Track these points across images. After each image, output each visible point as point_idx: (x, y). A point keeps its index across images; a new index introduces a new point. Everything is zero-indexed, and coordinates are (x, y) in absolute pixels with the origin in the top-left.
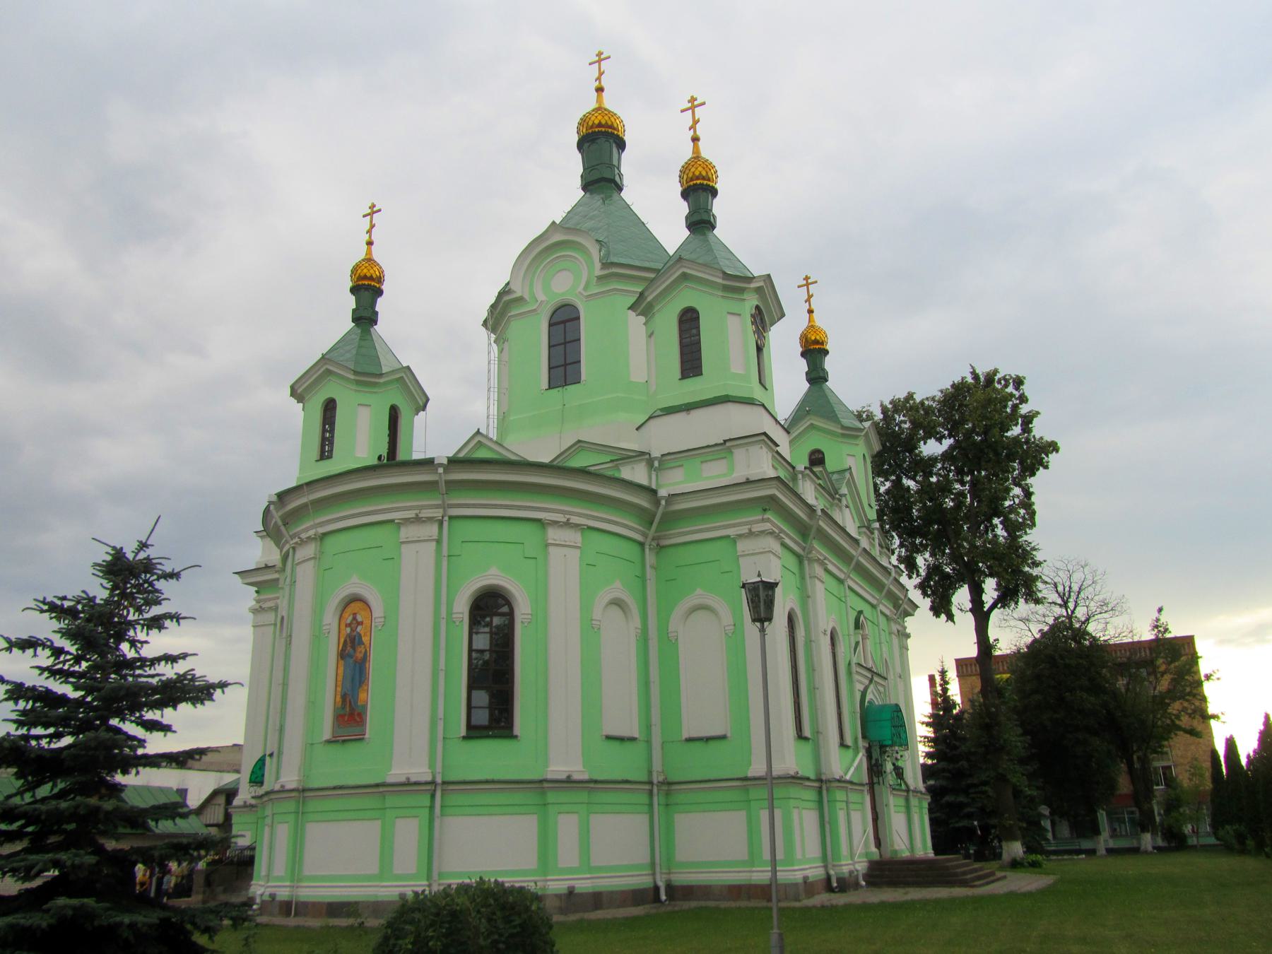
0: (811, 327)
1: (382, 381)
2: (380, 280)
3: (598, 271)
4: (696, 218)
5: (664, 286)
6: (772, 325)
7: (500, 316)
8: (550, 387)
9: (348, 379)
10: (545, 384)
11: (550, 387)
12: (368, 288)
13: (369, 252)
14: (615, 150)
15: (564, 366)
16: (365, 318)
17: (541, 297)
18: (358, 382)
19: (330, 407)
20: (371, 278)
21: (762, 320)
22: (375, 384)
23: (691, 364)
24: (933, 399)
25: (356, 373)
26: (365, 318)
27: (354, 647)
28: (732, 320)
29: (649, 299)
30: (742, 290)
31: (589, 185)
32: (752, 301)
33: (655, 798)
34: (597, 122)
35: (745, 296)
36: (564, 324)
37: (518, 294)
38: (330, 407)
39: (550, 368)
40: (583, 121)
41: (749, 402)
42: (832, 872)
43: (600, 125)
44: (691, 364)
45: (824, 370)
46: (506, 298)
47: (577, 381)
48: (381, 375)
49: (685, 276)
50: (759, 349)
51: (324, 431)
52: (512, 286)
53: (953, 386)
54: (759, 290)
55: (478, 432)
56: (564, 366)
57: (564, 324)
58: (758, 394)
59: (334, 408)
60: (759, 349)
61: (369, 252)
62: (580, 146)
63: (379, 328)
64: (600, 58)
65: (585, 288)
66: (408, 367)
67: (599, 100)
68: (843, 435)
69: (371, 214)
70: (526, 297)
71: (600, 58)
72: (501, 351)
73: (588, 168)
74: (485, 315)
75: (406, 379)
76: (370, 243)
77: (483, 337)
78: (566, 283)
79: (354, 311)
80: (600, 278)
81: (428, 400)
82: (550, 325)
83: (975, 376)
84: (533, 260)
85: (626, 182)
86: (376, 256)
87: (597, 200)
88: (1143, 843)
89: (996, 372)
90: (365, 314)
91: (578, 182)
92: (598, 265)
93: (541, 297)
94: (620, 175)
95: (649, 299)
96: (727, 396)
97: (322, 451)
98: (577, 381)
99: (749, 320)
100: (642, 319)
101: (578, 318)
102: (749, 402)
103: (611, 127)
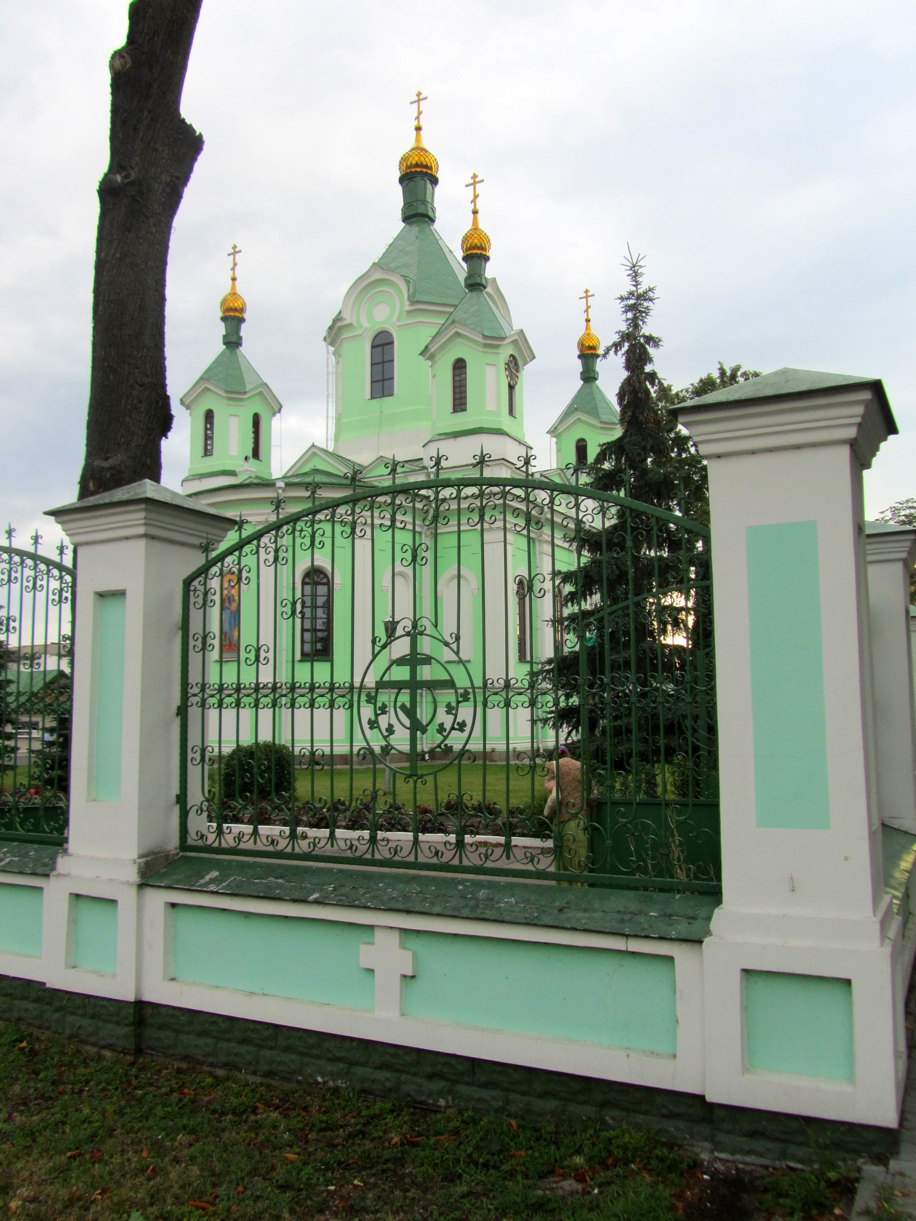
0: (588, 335)
1: (246, 397)
2: (242, 310)
3: (407, 307)
4: (471, 281)
5: (440, 343)
6: (525, 364)
7: (336, 333)
8: (372, 398)
9: (221, 396)
10: (369, 396)
11: (372, 398)
12: (234, 318)
13: (234, 287)
14: (429, 186)
15: (382, 382)
16: (233, 342)
17: (366, 324)
18: (229, 399)
19: (209, 416)
20: (236, 310)
21: (516, 364)
22: (241, 400)
23: (459, 403)
24: (687, 391)
25: (227, 392)
26: (233, 342)
27: (229, 603)
28: (490, 371)
29: (432, 351)
30: (497, 346)
31: (408, 218)
32: (506, 352)
33: (424, 698)
34: (414, 162)
35: (500, 351)
36: (382, 346)
37: (348, 322)
38: (209, 416)
39: (372, 382)
40: (404, 159)
41: (499, 432)
42: (541, 746)
43: (417, 165)
44: (459, 403)
45: (594, 371)
46: (339, 324)
47: (391, 394)
48: (245, 393)
49: (457, 334)
50: (511, 388)
51: (206, 429)
52: (343, 315)
53: (701, 381)
54: (515, 342)
55: (313, 446)
56: (382, 382)
57: (382, 346)
58: (505, 422)
59: (212, 417)
60: (511, 388)
61: (234, 287)
62: (401, 181)
63: (244, 349)
64: (419, 99)
65: (398, 320)
66: (266, 384)
67: (418, 139)
68: (602, 428)
69: (234, 254)
70: (354, 323)
71: (419, 99)
72: (338, 363)
73: (408, 205)
74: (325, 334)
75: (265, 393)
76: (234, 279)
77: (323, 350)
78: (386, 312)
79: (224, 337)
80: (409, 312)
81: (281, 407)
82: (373, 347)
83: (723, 372)
84: (362, 290)
85: (438, 214)
86: (239, 291)
87: (415, 229)
88: (5, 781)
89: (738, 368)
90: (233, 339)
91: (399, 215)
92: (407, 303)
93: (366, 324)
94: (433, 210)
95: (432, 351)
96: (482, 428)
97: (206, 450)
98: (391, 394)
99: (502, 367)
100: (430, 363)
101: (392, 343)
102: (499, 432)
103: (426, 167)
